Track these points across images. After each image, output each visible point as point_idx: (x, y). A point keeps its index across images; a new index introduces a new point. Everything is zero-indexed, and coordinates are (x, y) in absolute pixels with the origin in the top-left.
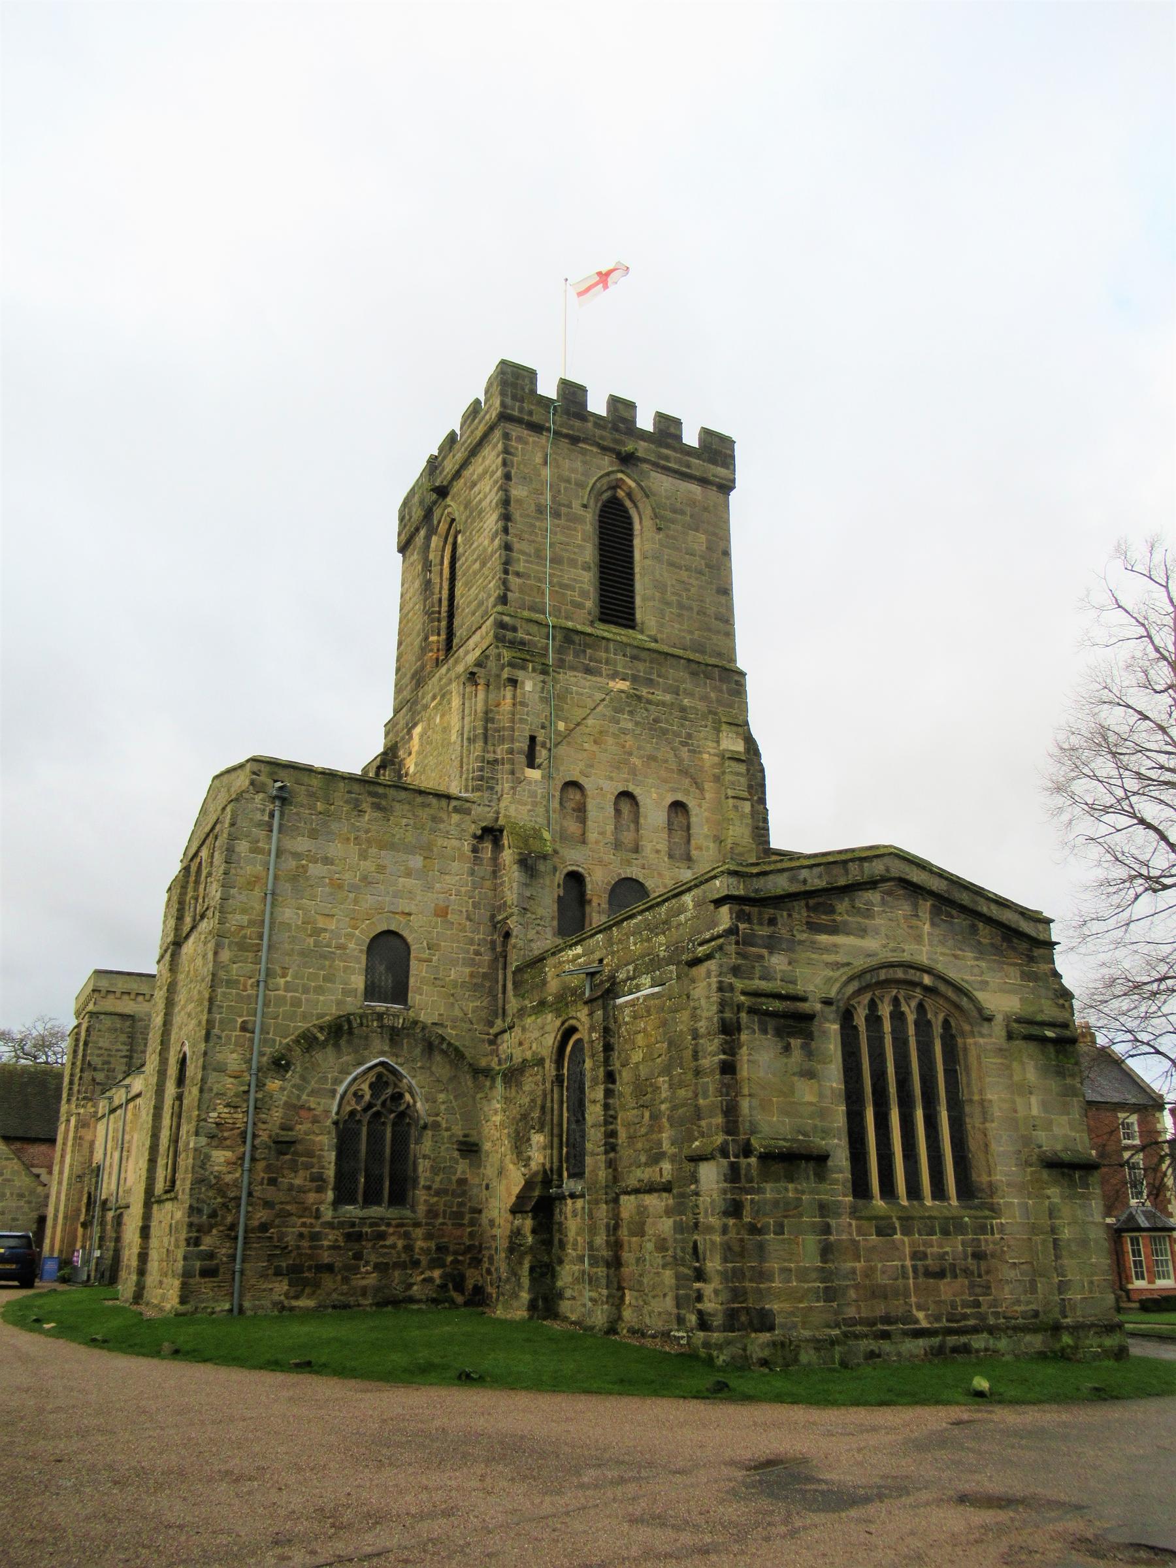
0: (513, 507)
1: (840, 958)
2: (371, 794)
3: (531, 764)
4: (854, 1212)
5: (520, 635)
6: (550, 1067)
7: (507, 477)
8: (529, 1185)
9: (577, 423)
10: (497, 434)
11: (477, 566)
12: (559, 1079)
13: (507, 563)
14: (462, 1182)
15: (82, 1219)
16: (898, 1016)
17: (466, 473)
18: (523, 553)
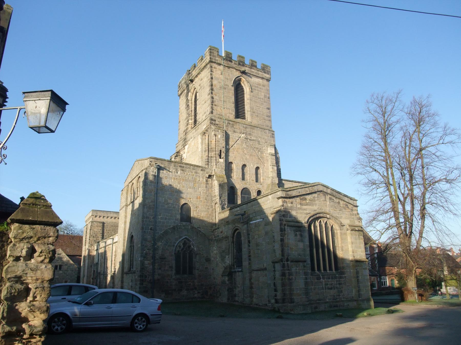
0: (213, 87)
1: (308, 212)
2: (180, 166)
3: (220, 158)
4: (312, 275)
5: (217, 122)
6: (230, 239)
7: (212, 78)
8: (226, 268)
9: (230, 63)
10: (209, 66)
11: (203, 102)
12: (233, 242)
13: (212, 102)
14: (206, 268)
15: (92, 277)
16: (320, 226)
17: (199, 76)
18: (217, 99)
